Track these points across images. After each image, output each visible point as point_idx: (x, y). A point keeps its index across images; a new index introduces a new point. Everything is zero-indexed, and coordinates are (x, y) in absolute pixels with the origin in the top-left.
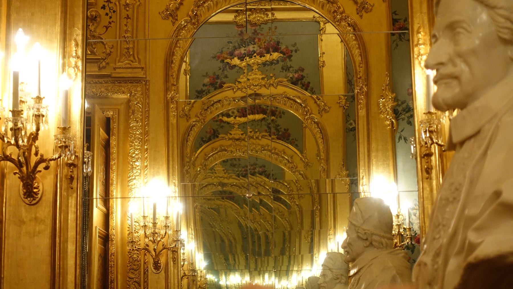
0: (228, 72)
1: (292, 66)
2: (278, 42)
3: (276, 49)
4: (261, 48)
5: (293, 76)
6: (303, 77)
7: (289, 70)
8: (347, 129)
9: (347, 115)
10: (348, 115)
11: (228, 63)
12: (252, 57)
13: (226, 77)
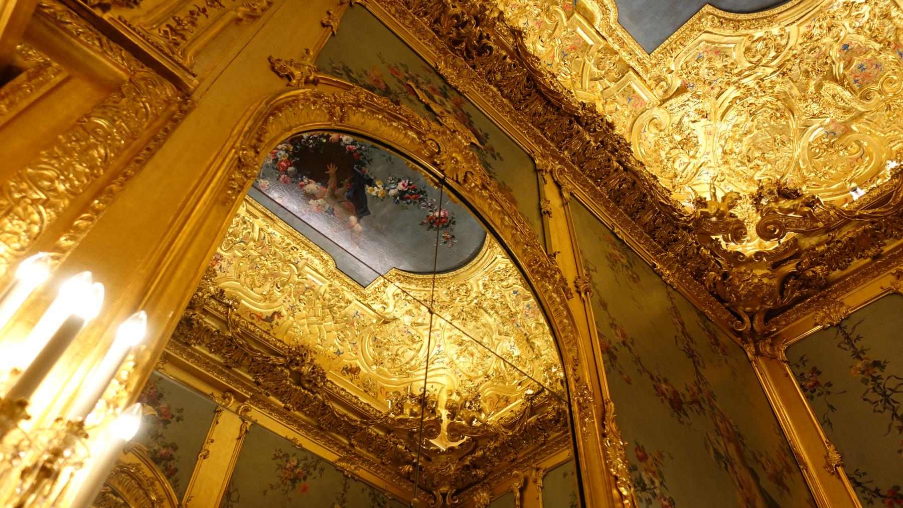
2: (161, 396)
5: (159, 450)
6: (171, 458)
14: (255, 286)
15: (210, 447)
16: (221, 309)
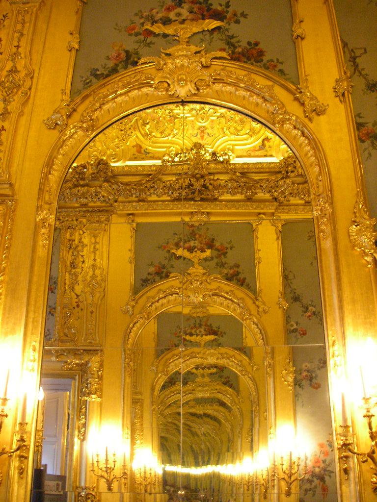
0: (174, 262)
1: (227, 262)
2: (213, 239)
3: (211, 246)
4: (201, 244)
5: (228, 272)
6: (238, 273)
7: (223, 266)
8: (287, 330)
9: (287, 316)
10: (289, 316)
11: (174, 253)
12: (192, 252)
13: (172, 266)
14: (239, 131)
15: (261, 254)
16: (219, 166)
